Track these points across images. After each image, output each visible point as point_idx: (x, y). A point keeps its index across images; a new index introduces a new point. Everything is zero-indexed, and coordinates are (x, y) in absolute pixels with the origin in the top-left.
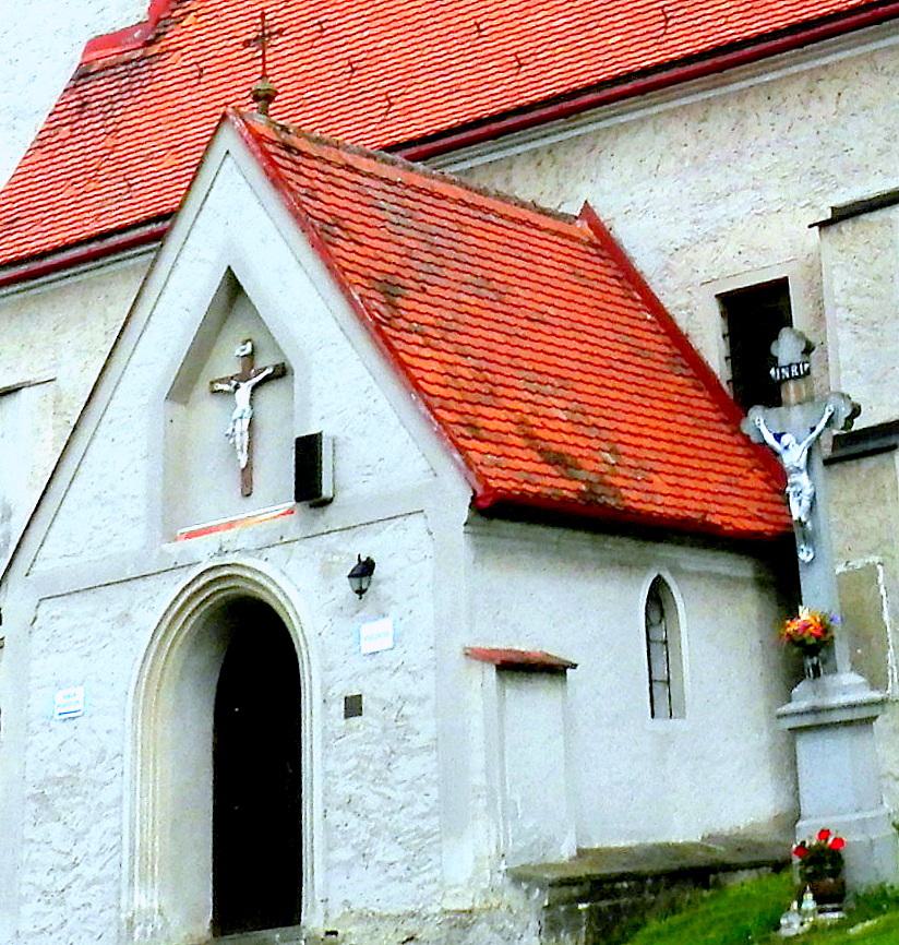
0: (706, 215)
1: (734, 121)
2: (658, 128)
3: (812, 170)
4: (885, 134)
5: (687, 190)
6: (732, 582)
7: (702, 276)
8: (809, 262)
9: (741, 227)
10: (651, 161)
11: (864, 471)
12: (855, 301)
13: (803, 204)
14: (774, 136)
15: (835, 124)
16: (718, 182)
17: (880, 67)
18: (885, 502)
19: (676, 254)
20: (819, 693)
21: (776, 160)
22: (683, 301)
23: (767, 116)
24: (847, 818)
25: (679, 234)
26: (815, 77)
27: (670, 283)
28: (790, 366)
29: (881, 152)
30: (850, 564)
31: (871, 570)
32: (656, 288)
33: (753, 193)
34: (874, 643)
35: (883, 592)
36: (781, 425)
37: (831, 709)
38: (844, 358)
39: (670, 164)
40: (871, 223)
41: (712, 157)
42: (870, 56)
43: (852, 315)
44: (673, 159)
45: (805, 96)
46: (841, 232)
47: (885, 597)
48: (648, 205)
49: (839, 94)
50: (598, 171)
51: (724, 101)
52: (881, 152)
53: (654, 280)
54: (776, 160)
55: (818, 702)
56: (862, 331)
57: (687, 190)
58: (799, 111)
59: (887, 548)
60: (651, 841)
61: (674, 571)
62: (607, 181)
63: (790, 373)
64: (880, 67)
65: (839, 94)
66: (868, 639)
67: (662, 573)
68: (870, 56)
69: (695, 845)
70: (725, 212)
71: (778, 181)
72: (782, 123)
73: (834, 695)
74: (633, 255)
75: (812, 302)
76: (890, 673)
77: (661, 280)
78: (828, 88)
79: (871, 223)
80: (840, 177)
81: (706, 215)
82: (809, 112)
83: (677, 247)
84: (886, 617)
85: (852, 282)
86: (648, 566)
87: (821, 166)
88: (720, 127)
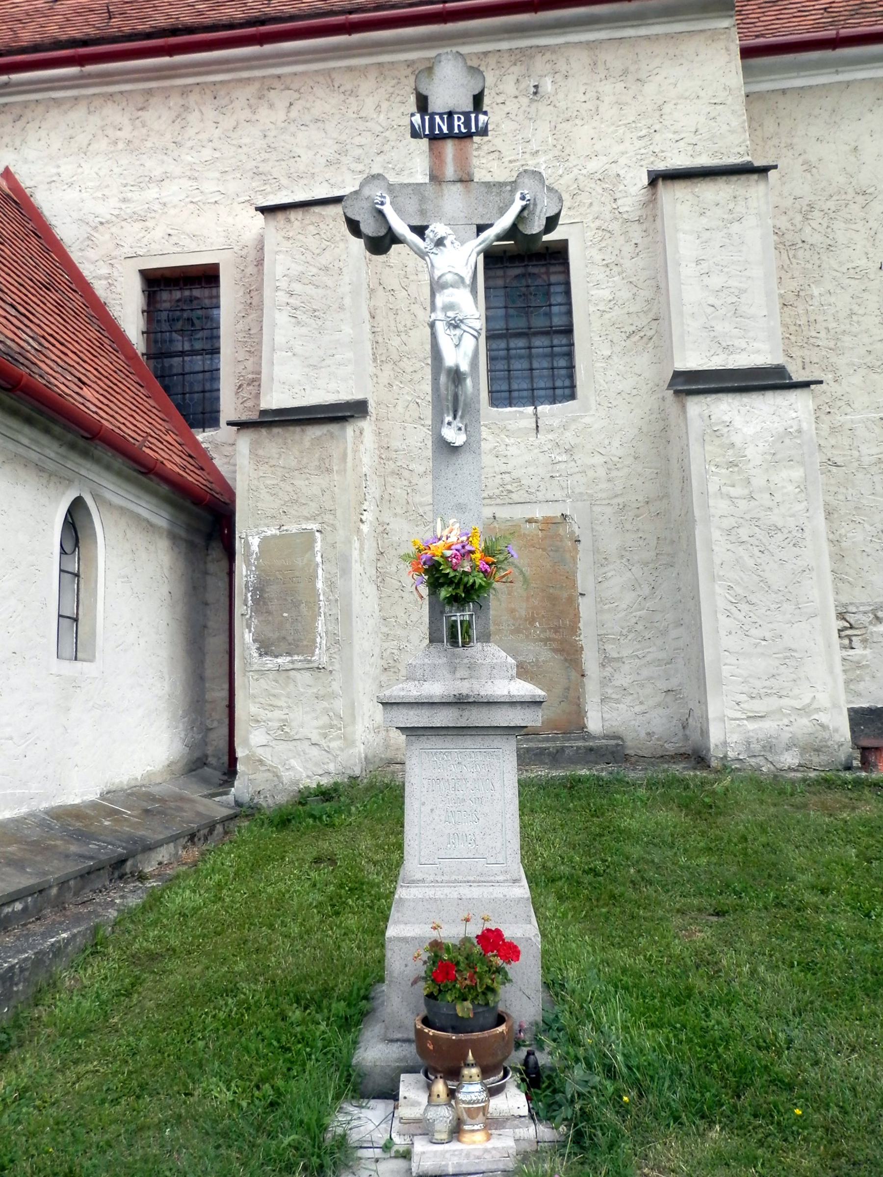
0: (135, 196)
1: (176, 114)
2: (92, 109)
3: (255, 170)
4: (336, 147)
5: (117, 170)
6: (150, 527)
7: (127, 251)
8: (243, 253)
9: (172, 212)
10: (82, 139)
11: (308, 438)
12: (297, 287)
13: (242, 199)
14: (217, 133)
15: (284, 130)
16: (154, 166)
17: (336, 86)
18: (329, 471)
19: (100, 228)
20: (460, 673)
21: (217, 154)
22: (104, 270)
23: (210, 114)
24: (498, 892)
25: (105, 210)
26: (267, 86)
27: (91, 254)
28: (450, 114)
29: (329, 163)
30: (284, 528)
31: (308, 538)
32: (75, 256)
33: (190, 183)
34: (303, 608)
35: (319, 559)
36: (423, 213)
37: (491, 703)
38: (279, 339)
39: (102, 144)
40: (323, 217)
41: (149, 144)
42: (329, 72)
43: (291, 301)
44: (105, 141)
45: (252, 101)
46: (289, 221)
47: (321, 565)
48: (75, 178)
49: (291, 104)
50: (24, 141)
51: (166, 93)
52: (329, 163)
53: (72, 249)
54: (217, 154)
55: (464, 688)
56: (302, 317)
57: (117, 170)
58: (247, 114)
59: (328, 518)
60: (44, 805)
61: (96, 497)
62: (30, 153)
63: (451, 126)
64: (336, 86)
65: (291, 104)
66: (296, 605)
67: (83, 495)
68: (329, 72)
69: (93, 805)
70: (157, 196)
71: (217, 175)
72: (227, 122)
73: (491, 677)
74: (53, 223)
75: (243, 289)
76: (318, 640)
77: (81, 250)
78: (281, 99)
79: (323, 217)
80: (284, 181)
81: (135, 196)
82: (257, 117)
83: (103, 220)
84: (320, 585)
85: (296, 269)
86: (67, 481)
87: (264, 168)
88: (160, 117)
